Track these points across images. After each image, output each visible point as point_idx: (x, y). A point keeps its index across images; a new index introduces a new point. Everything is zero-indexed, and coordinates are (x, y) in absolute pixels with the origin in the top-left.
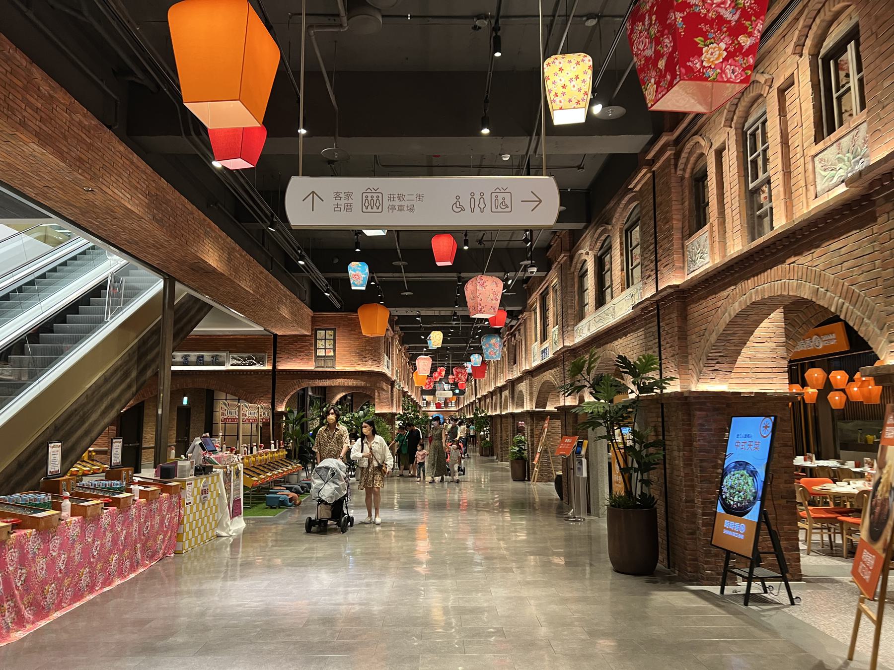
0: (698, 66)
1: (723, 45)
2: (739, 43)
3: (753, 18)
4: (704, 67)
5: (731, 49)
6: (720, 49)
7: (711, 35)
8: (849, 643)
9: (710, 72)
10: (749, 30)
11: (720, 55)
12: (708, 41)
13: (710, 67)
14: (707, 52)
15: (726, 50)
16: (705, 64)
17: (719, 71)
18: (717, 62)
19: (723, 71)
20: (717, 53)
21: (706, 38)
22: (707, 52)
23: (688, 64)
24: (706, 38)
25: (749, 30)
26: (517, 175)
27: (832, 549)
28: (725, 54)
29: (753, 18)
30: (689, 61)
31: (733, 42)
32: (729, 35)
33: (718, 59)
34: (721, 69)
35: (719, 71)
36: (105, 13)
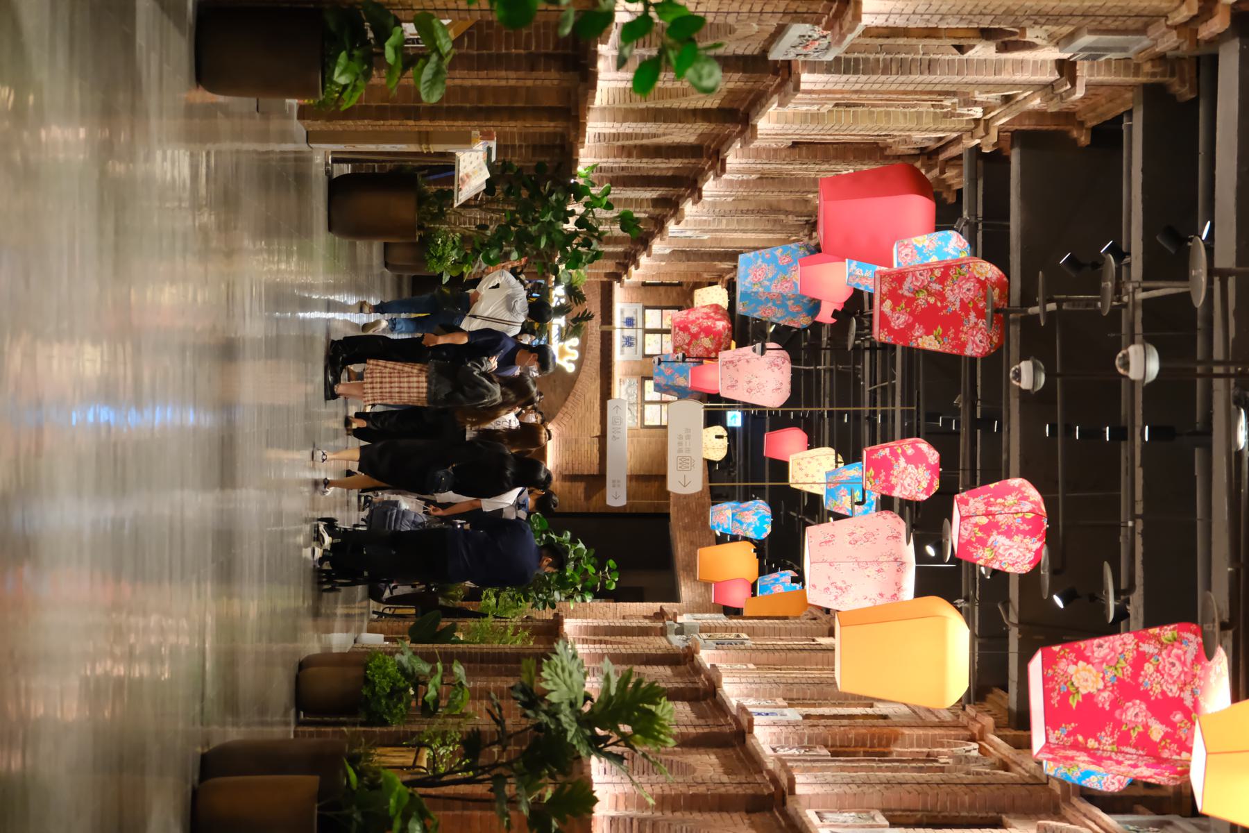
0: (1106, 694)
1: (1072, 669)
2: (1163, 738)
3: (1124, 728)
4: (1105, 687)
5: (1175, 746)
6: (1077, 672)
7: (1064, 689)
8: (659, 336)
9: (1109, 676)
10: (1141, 729)
11: (1084, 669)
12: (1072, 689)
13: (1103, 678)
14: (1086, 688)
15: (1076, 664)
16: (1101, 685)
17: (1104, 666)
18: (1094, 671)
19: (1103, 660)
20: (1083, 673)
21: (1069, 693)
22: (1086, 688)
23: (1107, 707)
24: (1069, 693)
25: (1141, 729)
26: (1009, 163)
27: (667, 332)
28: (1081, 663)
29: (1124, 728)
30: (1103, 708)
31: (1063, 657)
32: (1056, 663)
33: (1090, 672)
34: (1102, 663)
35: (1104, 666)
36: (1139, 473)
